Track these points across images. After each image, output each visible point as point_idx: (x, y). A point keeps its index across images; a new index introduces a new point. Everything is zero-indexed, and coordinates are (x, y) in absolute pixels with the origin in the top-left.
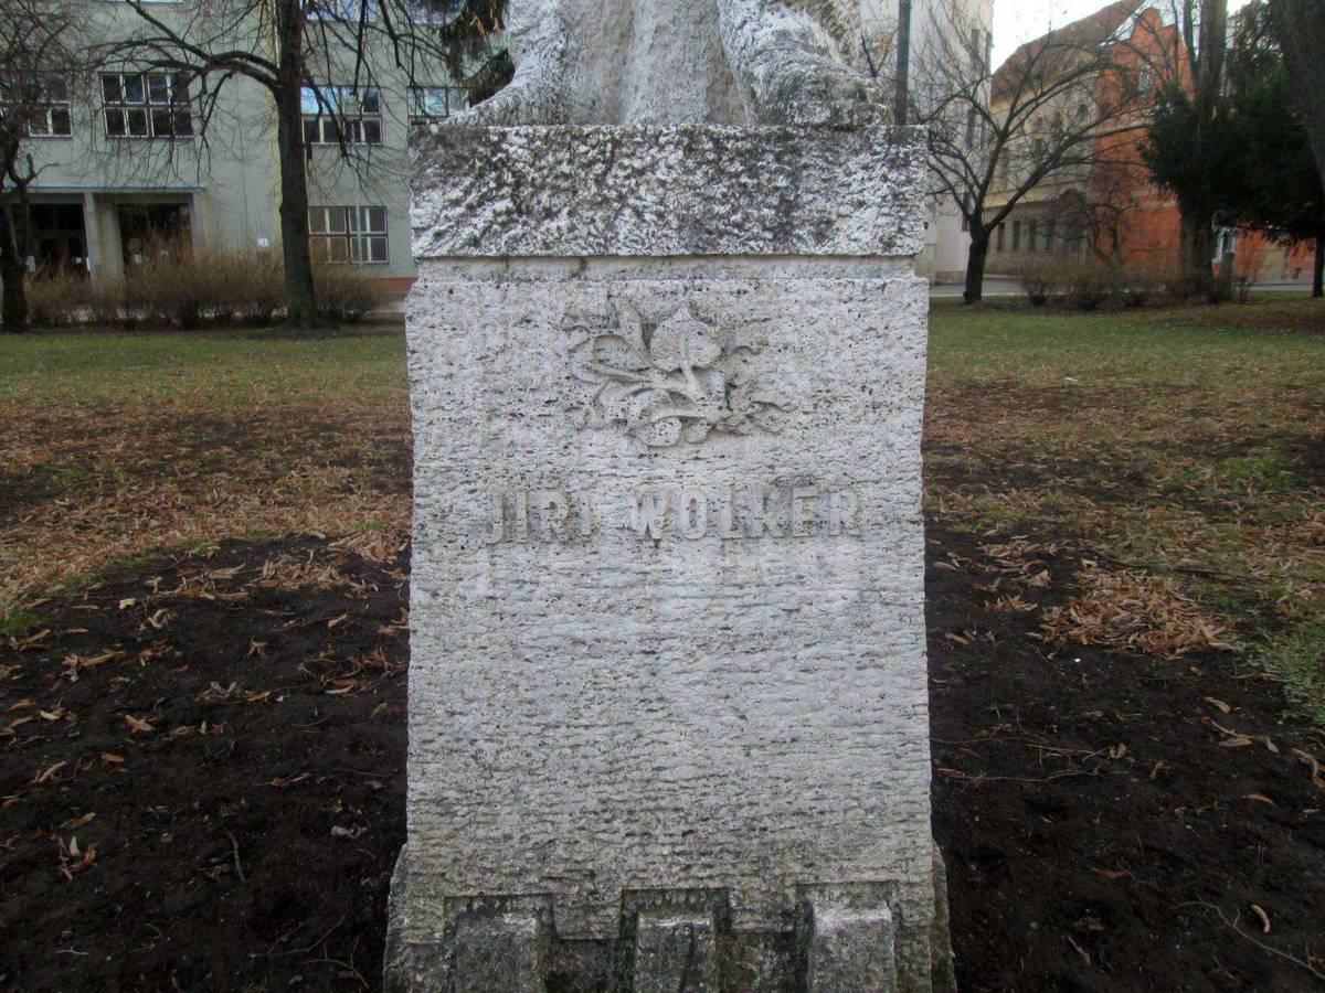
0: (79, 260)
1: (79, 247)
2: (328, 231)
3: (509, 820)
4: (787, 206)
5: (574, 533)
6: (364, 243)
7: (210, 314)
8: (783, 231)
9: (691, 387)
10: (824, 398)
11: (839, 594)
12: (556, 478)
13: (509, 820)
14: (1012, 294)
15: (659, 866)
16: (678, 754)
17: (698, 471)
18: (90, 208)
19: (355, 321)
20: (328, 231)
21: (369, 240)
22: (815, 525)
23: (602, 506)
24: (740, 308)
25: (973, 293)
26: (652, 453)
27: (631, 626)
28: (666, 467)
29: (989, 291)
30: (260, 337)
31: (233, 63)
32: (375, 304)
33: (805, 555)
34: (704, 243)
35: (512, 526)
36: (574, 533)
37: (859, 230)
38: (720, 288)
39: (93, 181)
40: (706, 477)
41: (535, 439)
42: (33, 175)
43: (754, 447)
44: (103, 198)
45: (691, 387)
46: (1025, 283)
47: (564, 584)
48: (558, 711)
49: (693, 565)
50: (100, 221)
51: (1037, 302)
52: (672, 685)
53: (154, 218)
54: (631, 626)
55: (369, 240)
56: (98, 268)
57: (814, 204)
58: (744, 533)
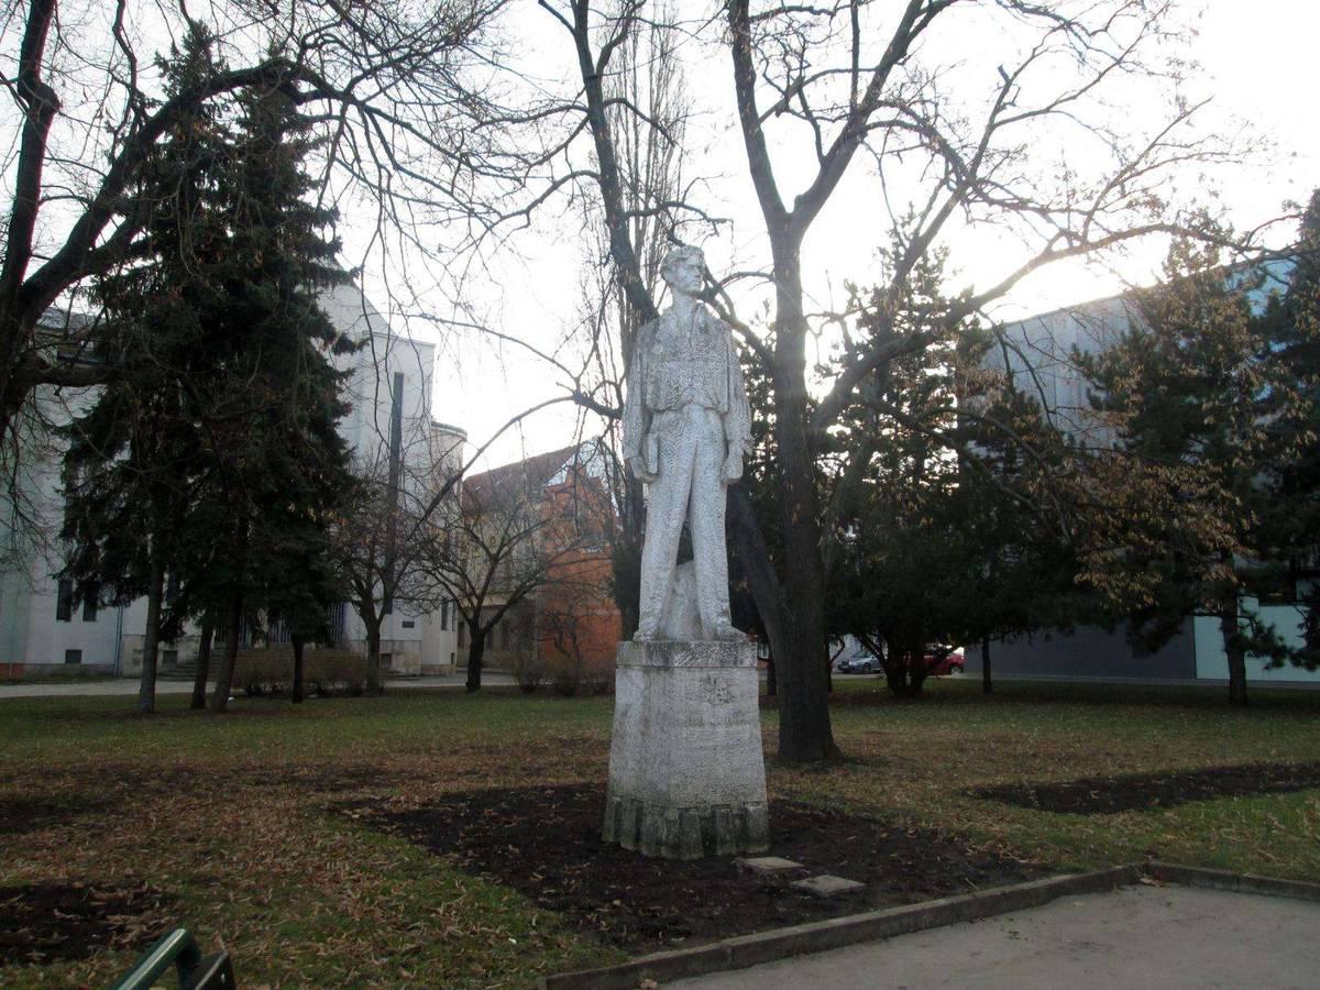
5: (701, 724)
8: (735, 663)
11: (747, 736)
12: (697, 712)
14: (506, 684)
15: (717, 799)
16: (721, 772)
23: (706, 718)
25: (473, 684)
26: (714, 706)
27: (711, 744)
28: (716, 709)
29: (487, 681)
33: (740, 728)
34: (723, 664)
37: (747, 662)
38: (725, 673)
40: (724, 711)
43: (730, 706)
46: (517, 675)
51: (529, 690)
52: (719, 756)
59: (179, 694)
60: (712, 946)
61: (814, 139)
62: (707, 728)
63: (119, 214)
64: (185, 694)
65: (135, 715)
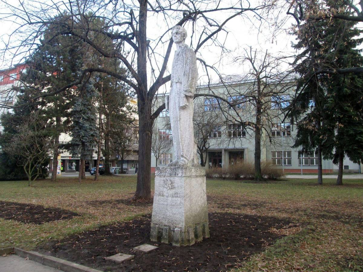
0: (220, 164)
1: (220, 161)
2: (276, 157)
3: (158, 218)
4: (176, 173)
5: (163, 196)
6: (303, 160)
7: (242, 177)
8: (175, 175)
9: (170, 185)
10: (178, 187)
11: (179, 202)
12: (162, 191)
13: (158, 218)
16: (168, 214)
17: (171, 192)
18: (223, 152)
19: (275, 180)
20: (276, 157)
21: (304, 159)
22: (177, 196)
23: (165, 194)
24: (173, 180)
27: (166, 203)
30: (246, 182)
31: (249, 124)
32: (280, 176)
33: (176, 199)
34: (171, 175)
35: (160, 195)
36: (163, 196)
37: (180, 175)
38: (172, 179)
39: (223, 146)
40: (172, 192)
41: (161, 188)
42: (209, 147)
43: (174, 190)
44: (225, 150)
45: (170, 185)
47: (162, 199)
48: (161, 209)
49: (170, 199)
50: (225, 156)
52: (168, 208)
53: (237, 154)
54: (166, 203)
55: (304, 159)
56: (223, 165)
57: (177, 173)
58: (173, 197)
59: (356, 179)
60: (41, 255)
61: (226, 10)
62: (165, 197)
63: (54, 117)
64: (335, 179)
65: (316, 185)
